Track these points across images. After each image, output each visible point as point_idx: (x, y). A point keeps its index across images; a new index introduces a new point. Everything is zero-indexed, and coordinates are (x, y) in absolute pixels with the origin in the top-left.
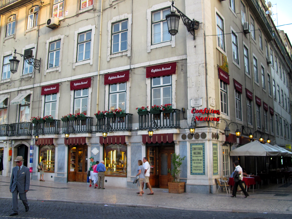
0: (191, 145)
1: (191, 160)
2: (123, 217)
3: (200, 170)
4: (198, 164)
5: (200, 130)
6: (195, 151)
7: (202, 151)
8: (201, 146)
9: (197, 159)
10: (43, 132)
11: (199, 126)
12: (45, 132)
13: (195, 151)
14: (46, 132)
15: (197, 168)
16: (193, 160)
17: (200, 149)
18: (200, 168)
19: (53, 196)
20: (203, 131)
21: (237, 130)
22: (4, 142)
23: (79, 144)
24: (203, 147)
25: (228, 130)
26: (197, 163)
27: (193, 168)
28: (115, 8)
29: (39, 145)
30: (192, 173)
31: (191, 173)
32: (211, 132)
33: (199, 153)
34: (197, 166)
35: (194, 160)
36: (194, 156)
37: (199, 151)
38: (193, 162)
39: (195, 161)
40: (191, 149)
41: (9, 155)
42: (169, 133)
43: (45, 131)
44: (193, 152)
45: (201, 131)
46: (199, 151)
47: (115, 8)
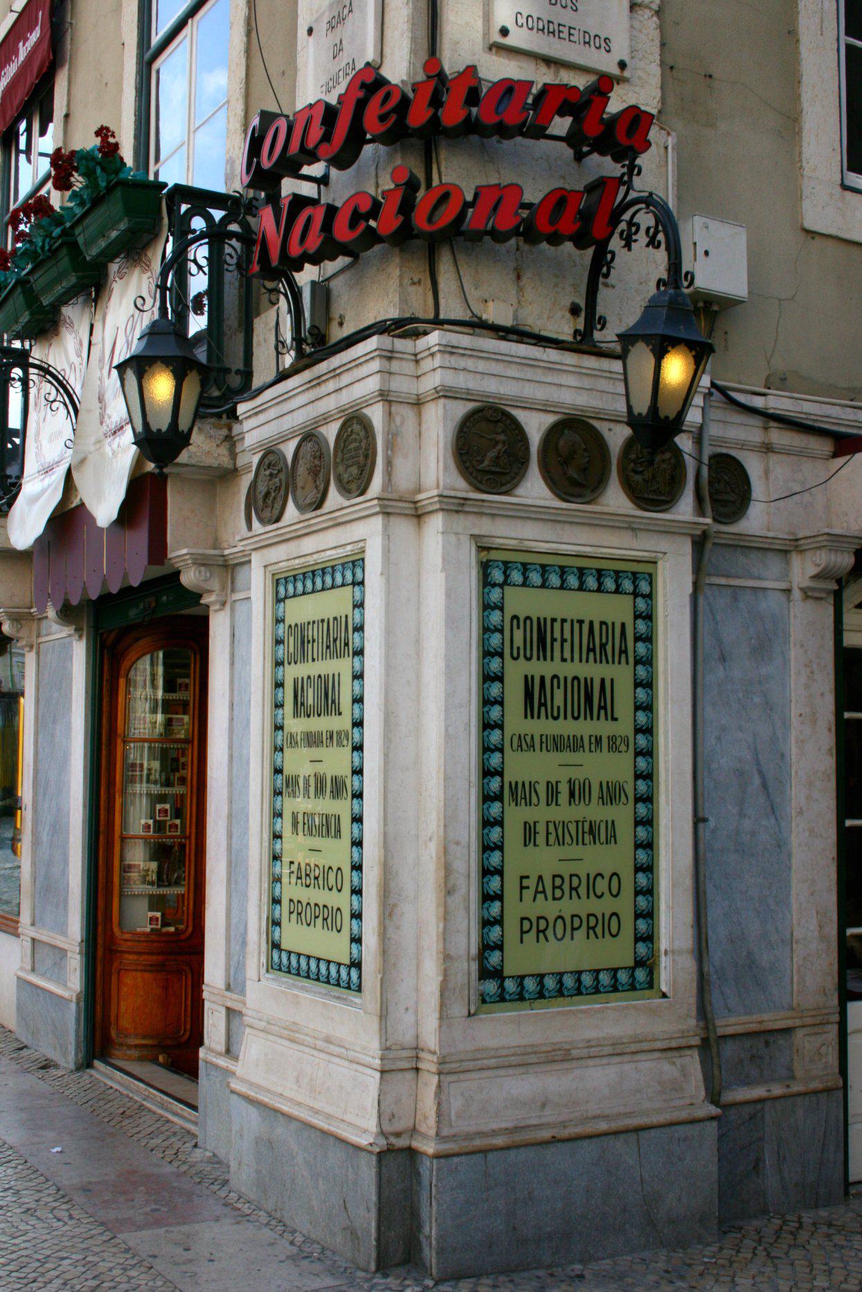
0: (497, 576)
6: (539, 668)
9: (563, 776)
13: (539, 668)
16: (514, 789)
20: (346, 398)
26: (559, 834)
28: (706, 253)
35: (522, 793)
36: (525, 743)
37: (593, 671)
38: (515, 816)
39: (540, 813)
40: (495, 640)
44: (516, 672)
46: (593, 671)
47: (706, 253)
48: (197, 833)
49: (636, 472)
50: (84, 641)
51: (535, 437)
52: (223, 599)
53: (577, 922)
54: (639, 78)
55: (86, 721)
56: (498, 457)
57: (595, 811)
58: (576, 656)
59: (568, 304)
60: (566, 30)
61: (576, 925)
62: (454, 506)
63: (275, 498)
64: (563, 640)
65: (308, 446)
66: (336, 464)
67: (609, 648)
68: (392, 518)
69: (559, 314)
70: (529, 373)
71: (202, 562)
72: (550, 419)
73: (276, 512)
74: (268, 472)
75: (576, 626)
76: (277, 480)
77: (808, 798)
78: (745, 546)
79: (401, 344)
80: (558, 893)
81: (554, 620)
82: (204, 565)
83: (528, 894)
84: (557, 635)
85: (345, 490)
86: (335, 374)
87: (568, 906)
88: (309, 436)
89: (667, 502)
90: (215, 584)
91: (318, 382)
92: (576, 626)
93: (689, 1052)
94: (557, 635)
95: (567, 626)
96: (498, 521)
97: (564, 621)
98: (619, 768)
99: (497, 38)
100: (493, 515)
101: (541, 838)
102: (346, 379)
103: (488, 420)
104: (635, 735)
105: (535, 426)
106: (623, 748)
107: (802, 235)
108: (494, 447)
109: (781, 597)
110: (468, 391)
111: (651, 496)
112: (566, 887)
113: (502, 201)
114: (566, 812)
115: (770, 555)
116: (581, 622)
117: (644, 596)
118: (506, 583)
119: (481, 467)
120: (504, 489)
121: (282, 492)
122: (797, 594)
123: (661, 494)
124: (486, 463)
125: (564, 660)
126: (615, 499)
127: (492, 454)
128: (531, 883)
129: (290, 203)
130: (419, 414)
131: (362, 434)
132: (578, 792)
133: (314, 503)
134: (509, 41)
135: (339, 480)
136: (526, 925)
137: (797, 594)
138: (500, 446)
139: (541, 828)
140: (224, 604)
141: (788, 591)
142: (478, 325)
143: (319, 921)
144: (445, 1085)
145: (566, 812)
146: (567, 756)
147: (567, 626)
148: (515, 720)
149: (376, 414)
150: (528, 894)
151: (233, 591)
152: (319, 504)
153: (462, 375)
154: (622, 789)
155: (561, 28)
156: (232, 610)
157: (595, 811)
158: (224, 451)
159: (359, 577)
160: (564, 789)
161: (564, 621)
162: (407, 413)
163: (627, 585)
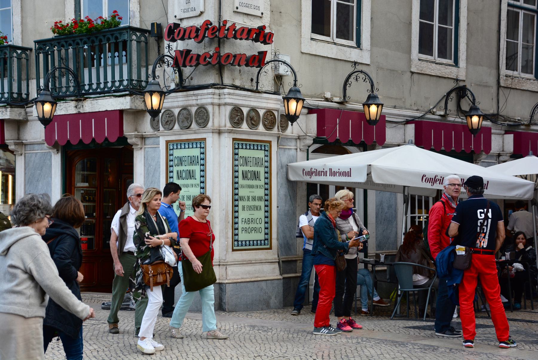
0: (237, 147)
1: (237, 197)
2: (111, 348)
3: (255, 230)
4: (252, 212)
5: (194, 98)
7: (197, 169)
8: (195, 152)
9: (251, 195)
10: (79, 85)
11: (196, 82)
12: (87, 87)
14: (90, 85)
15: (251, 225)
16: (240, 197)
17: (192, 161)
18: (258, 226)
19: (379, 353)
20: (199, 102)
21: (369, 97)
22: (424, 115)
23: (74, 142)
24: (201, 153)
25: (299, 96)
26: (250, 208)
27: (241, 225)
29: (64, 143)
30: (238, 241)
31: (236, 243)
32: (226, 104)
33: (256, 175)
34: (250, 217)
35: (242, 199)
36: (243, 187)
37: (191, 168)
38: (241, 204)
39: (246, 203)
40: (237, 162)
41: (308, 182)
42: (109, 108)
43: (87, 82)
44: (241, 169)
45: (194, 102)
46: (191, 168)
48: (270, 188)
49: (266, 121)
50: (60, 154)
51: (245, 114)
52: (142, 147)
53: (253, 229)
54: (265, 16)
55: (61, 181)
56: (238, 119)
57: (257, 203)
58: (342, 173)
59: (250, 78)
60: (250, 5)
61: (253, 229)
62: (230, 132)
63: (170, 123)
64: (250, 162)
65: (185, 112)
66: (195, 118)
67: (259, 163)
68: (214, 133)
69: (248, 82)
70: (244, 98)
71: (136, 137)
72: (248, 109)
73: (171, 127)
74: (168, 116)
75: (253, 158)
76: (171, 118)
77: (300, 202)
78: (288, 138)
79: (217, 91)
80: (249, 222)
81: (248, 157)
82: (137, 137)
83: (243, 223)
84: (249, 161)
85: (198, 124)
86: (197, 95)
87: (251, 225)
88: (185, 109)
89: (272, 128)
90: (139, 143)
91: (187, 96)
92: (253, 158)
93: (276, 263)
94: (249, 161)
95: (251, 158)
96: (238, 134)
97: (250, 157)
98: (261, 192)
99: (236, 10)
100: (237, 133)
101: (246, 209)
102: (199, 97)
103: (236, 110)
104: (265, 184)
105: (245, 111)
106: (262, 188)
107: (301, 54)
108: (237, 116)
109: (295, 151)
110: (232, 103)
111: (269, 127)
112: (250, 221)
113: (242, 59)
114: (251, 203)
115: (292, 140)
116: (254, 158)
117: (267, 151)
118: (238, 149)
119: (234, 122)
120: (239, 127)
121: (173, 122)
122: (298, 150)
123: (271, 126)
124: (236, 121)
125: (250, 166)
126: (261, 128)
127: (237, 118)
128: (244, 220)
129: (186, 51)
130: (219, 107)
131: (205, 112)
132: (254, 199)
133: (187, 126)
134: (238, 10)
135: (196, 122)
136: (243, 229)
137: (298, 150)
138: (238, 116)
139: (246, 207)
140: (141, 148)
141: (297, 149)
142: (236, 88)
143: (314, 174)
144: (227, 267)
145: (251, 203)
146: (251, 190)
147: (251, 158)
148: (241, 181)
149: (210, 108)
150: (243, 223)
151: (145, 144)
152: (188, 128)
153: (231, 99)
154: (262, 197)
155: (249, 5)
156: (144, 150)
157: (257, 203)
158: (143, 104)
159: (203, 146)
160: (185, 197)
161: (250, 157)
162: (216, 108)
163: (263, 148)
